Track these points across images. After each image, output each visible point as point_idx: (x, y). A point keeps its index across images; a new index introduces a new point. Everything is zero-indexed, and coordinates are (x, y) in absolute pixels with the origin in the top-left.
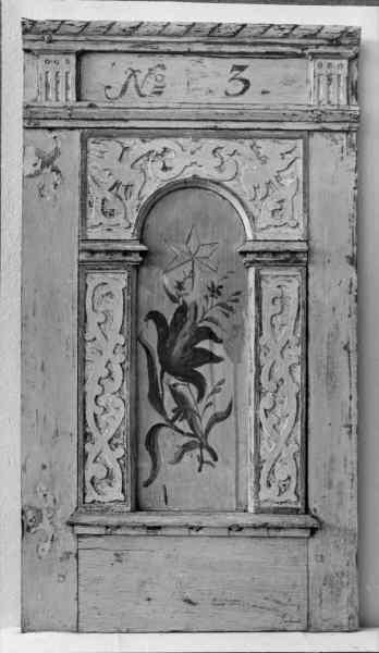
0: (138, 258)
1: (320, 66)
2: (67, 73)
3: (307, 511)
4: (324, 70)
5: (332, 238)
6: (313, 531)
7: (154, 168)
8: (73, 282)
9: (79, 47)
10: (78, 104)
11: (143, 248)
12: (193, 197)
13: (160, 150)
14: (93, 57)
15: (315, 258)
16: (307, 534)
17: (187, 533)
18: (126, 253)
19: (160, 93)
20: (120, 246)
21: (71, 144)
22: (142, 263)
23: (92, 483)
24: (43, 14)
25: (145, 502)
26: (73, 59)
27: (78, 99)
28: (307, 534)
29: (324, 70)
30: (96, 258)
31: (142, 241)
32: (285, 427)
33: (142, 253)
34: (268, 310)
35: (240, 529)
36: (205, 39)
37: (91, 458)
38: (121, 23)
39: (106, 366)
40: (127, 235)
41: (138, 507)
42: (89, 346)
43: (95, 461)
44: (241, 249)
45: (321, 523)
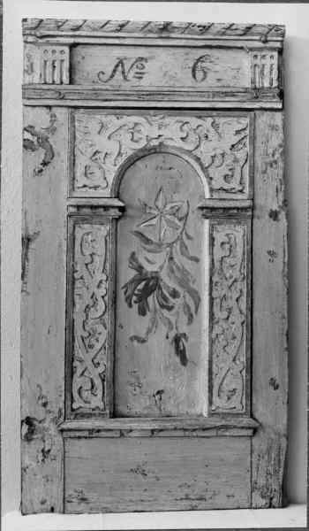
0: (115, 213)
1: (256, 56)
2: (272, 66)
3: (252, 416)
4: (50, 56)
5: (269, 200)
6: (255, 431)
7: (125, 137)
8: (63, 233)
9: (72, 40)
10: (71, 87)
11: (121, 204)
12: (155, 160)
13: (131, 126)
14: (79, 48)
15: (257, 212)
16: (250, 432)
17: (215, 434)
18: (106, 208)
19: (141, 78)
20: (101, 202)
21: (62, 115)
22: (120, 217)
23: (79, 393)
24: (34, 14)
25: (122, 409)
26: (67, 49)
27: (71, 82)
28: (250, 432)
29: (258, 61)
30: (84, 213)
31: (118, 197)
32: (232, 350)
33: (122, 209)
34: (218, 253)
35: (99, 431)
36: (156, 36)
37: (79, 371)
38: (237, 25)
39: (92, 297)
40: (107, 193)
41: (115, 415)
42: (78, 284)
43: (82, 374)
44: (200, 205)
45: (261, 425)
